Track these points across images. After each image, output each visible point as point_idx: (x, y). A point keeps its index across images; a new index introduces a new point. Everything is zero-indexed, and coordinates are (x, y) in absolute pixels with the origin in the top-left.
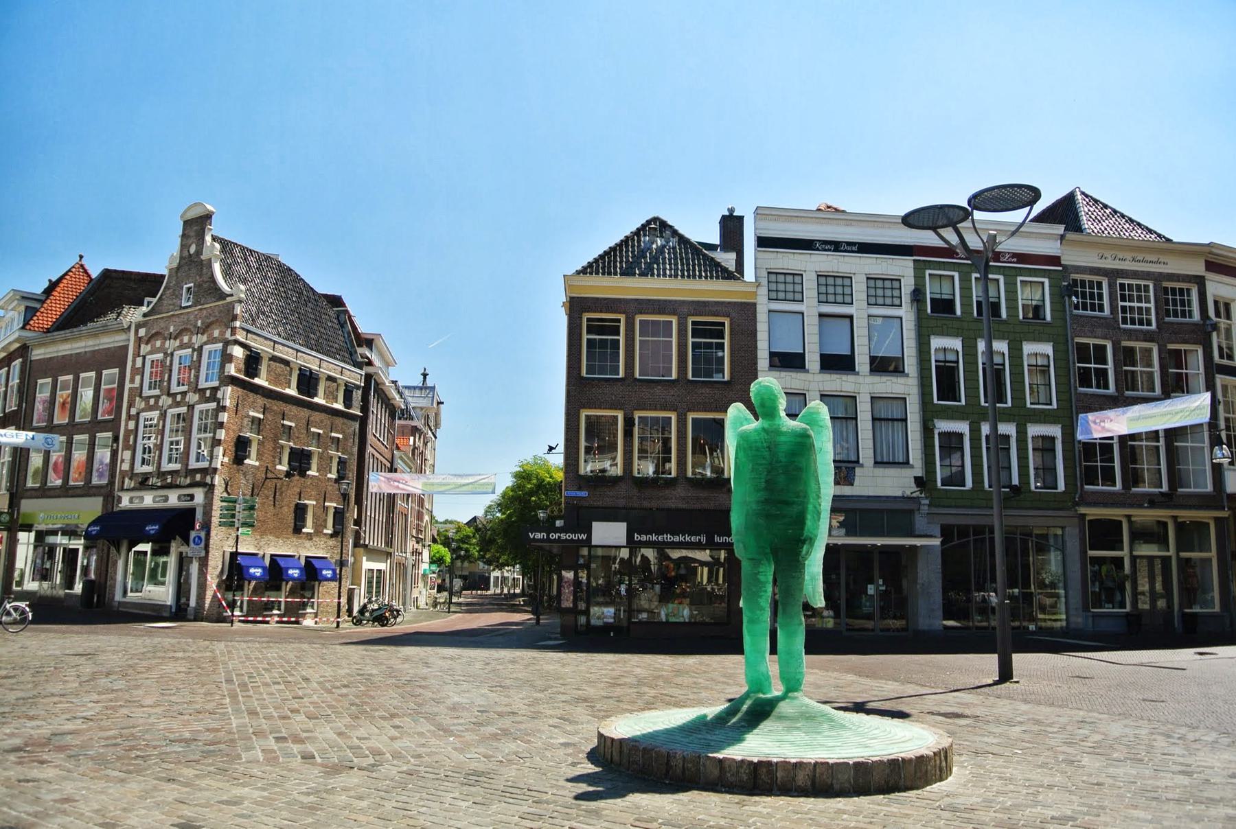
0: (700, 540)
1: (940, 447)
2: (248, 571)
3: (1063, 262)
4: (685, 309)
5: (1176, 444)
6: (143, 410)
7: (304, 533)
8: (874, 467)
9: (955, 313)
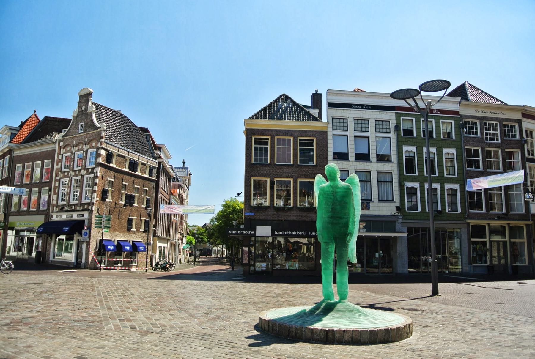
0: (303, 234)
1: (407, 193)
2: (107, 247)
3: (460, 114)
4: (296, 134)
5: (509, 192)
6: (62, 178)
7: (132, 231)
8: (378, 202)
9: (413, 136)
